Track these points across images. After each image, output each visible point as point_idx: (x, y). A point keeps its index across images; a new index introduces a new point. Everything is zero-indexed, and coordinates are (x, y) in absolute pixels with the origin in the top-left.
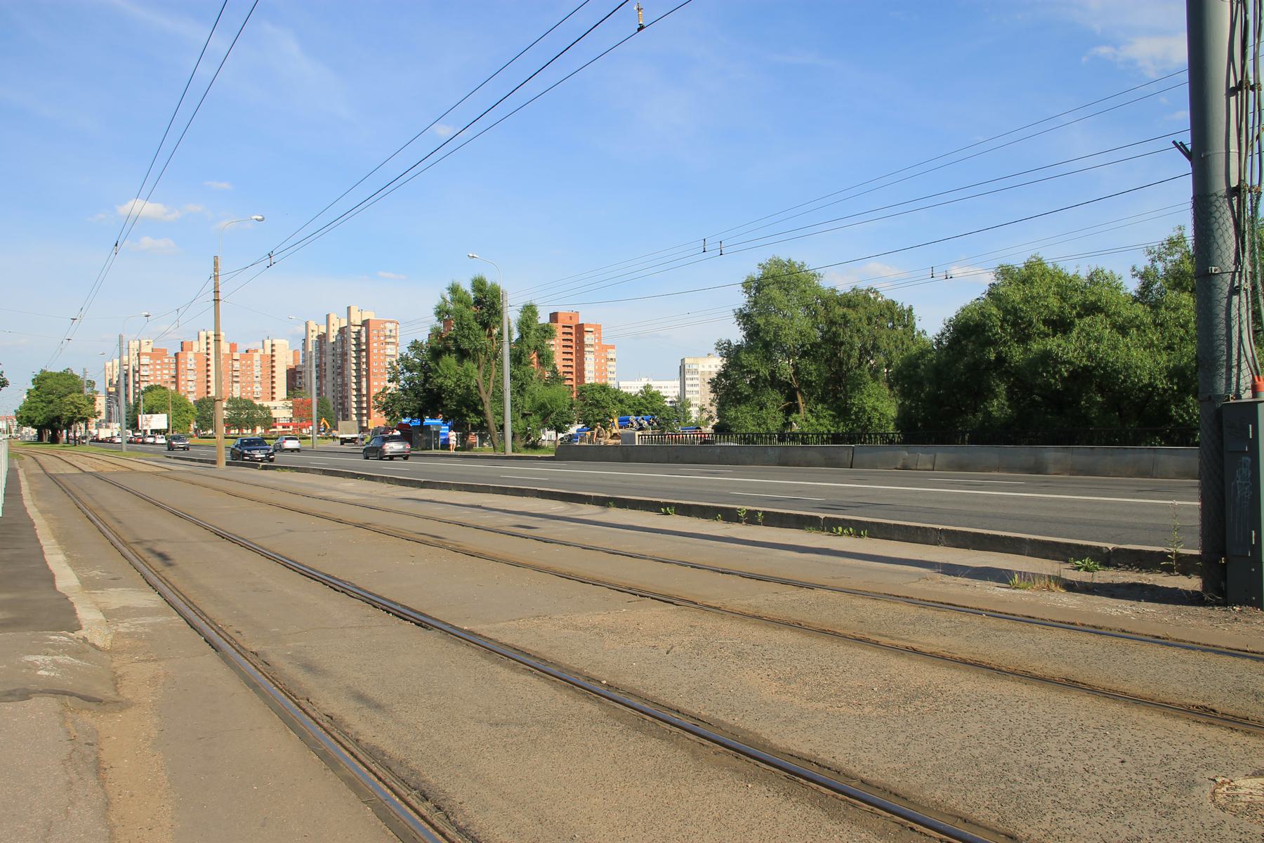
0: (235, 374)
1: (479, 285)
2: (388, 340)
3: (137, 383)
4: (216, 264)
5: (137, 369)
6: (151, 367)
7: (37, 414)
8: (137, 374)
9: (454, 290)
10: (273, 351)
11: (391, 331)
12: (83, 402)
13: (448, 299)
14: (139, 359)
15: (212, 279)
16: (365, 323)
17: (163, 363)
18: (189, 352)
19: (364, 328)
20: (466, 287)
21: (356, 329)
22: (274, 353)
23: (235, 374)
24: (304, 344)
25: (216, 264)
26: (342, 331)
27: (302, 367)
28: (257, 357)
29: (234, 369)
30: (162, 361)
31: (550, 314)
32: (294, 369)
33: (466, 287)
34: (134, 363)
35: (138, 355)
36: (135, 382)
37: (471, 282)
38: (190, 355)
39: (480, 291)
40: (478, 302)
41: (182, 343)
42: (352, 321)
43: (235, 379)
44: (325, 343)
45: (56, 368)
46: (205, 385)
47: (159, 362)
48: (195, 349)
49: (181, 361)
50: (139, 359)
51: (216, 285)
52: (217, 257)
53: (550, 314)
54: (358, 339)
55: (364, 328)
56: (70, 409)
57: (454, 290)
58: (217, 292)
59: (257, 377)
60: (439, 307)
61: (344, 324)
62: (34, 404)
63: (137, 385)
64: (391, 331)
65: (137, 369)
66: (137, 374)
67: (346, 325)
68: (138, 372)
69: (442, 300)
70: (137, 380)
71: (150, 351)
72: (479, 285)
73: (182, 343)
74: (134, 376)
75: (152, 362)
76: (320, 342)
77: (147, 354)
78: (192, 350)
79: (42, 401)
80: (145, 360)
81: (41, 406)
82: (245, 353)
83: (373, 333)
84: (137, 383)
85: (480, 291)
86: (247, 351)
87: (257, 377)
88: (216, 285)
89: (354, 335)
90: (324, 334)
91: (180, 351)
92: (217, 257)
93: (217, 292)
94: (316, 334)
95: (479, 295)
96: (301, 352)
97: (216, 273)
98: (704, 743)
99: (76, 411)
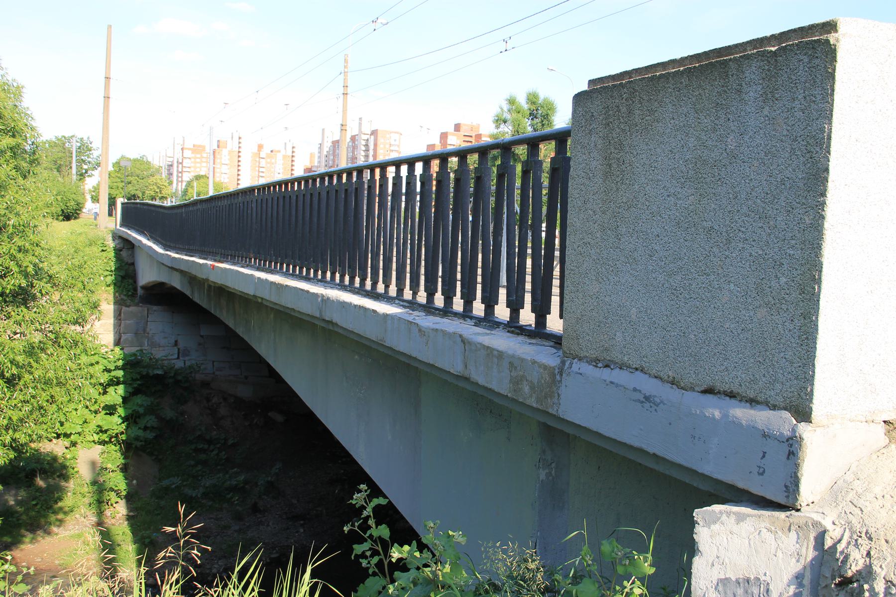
0: (261, 170)
1: (532, 99)
2: (392, 148)
3: (180, 172)
4: (346, 61)
5: (181, 161)
6: (193, 160)
7: (118, 192)
8: (180, 166)
9: (511, 101)
10: (293, 152)
11: (395, 140)
12: (165, 184)
13: (505, 109)
14: (183, 153)
15: (342, 74)
16: (374, 133)
17: (202, 157)
18: (224, 149)
19: (372, 137)
20: (522, 101)
21: (365, 137)
22: (294, 154)
23: (261, 170)
24: (320, 148)
25: (346, 61)
26: (353, 139)
27: (317, 167)
28: (280, 156)
29: (260, 166)
30: (201, 155)
31: (428, 146)
32: (311, 169)
33: (522, 101)
34: (178, 155)
35: (182, 149)
36: (178, 172)
37: (525, 95)
38: (225, 152)
39: (533, 103)
40: (533, 115)
41: (218, 141)
42: (363, 130)
43: (261, 174)
44: (338, 147)
45: (133, 155)
46: (236, 177)
47: (199, 156)
48: (229, 147)
49: (217, 156)
50: (183, 153)
51: (345, 80)
52: (347, 55)
53: (428, 146)
54: (367, 145)
55: (372, 137)
56: (154, 188)
57: (511, 101)
58: (346, 87)
59: (279, 173)
60: (497, 116)
61: (355, 132)
62: (115, 184)
63: (180, 175)
64: (395, 140)
65: (181, 161)
66: (180, 166)
67: (357, 133)
68: (181, 163)
69: (500, 110)
70: (180, 170)
71: (192, 147)
72: (532, 99)
73: (218, 141)
74: (178, 167)
75: (193, 155)
76: (334, 146)
77: (189, 149)
78: (226, 148)
79: (122, 182)
80: (187, 153)
81: (121, 186)
82: (270, 152)
83: (381, 140)
84: (180, 172)
85: (533, 103)
86: (272, 151)
87: (279, 173)
88: (345, 80)
89: (363, 143)
90: (338, 141)
91: (216, 148)
92: (347, 55)
93: (346, 87)
94: (330, 141)
95: (533, 107)
96: (317, 155)
97: (346, 70)
98: (809, 550)
99: (158, 190)
